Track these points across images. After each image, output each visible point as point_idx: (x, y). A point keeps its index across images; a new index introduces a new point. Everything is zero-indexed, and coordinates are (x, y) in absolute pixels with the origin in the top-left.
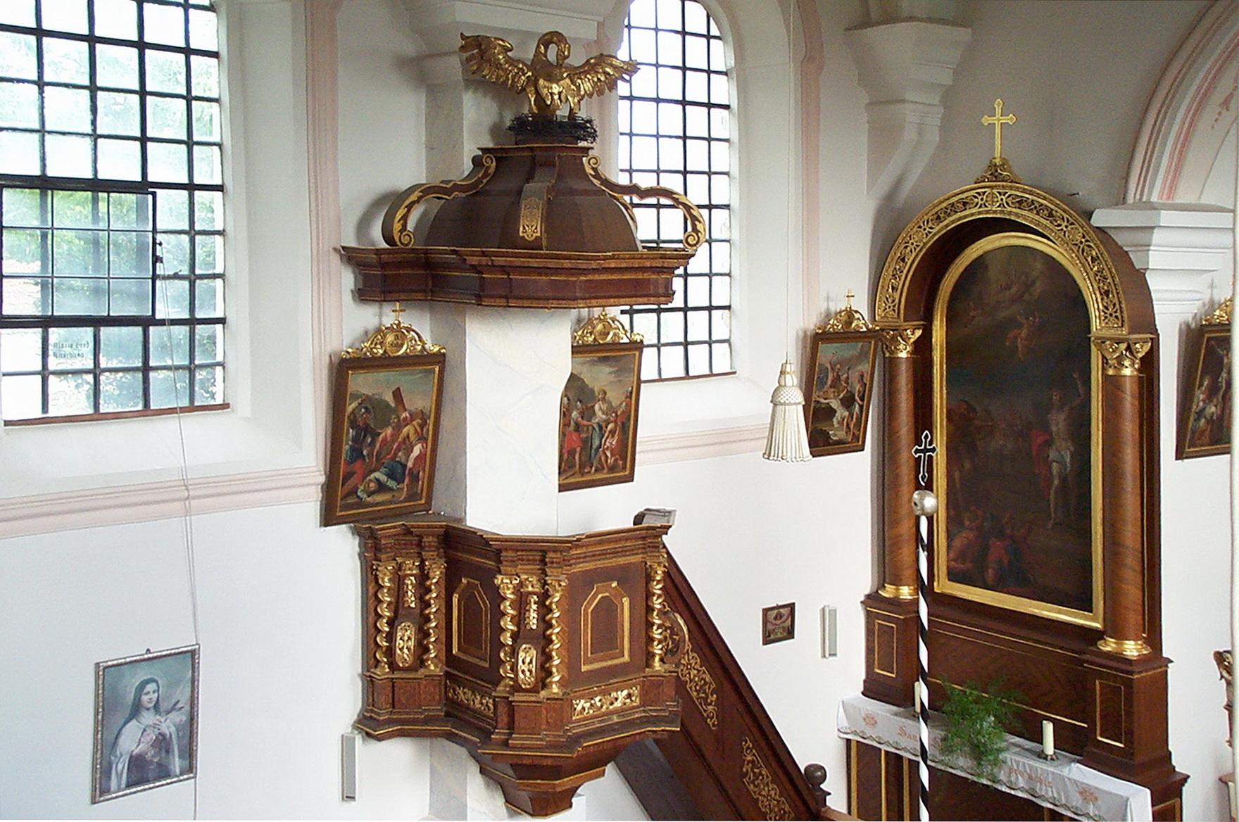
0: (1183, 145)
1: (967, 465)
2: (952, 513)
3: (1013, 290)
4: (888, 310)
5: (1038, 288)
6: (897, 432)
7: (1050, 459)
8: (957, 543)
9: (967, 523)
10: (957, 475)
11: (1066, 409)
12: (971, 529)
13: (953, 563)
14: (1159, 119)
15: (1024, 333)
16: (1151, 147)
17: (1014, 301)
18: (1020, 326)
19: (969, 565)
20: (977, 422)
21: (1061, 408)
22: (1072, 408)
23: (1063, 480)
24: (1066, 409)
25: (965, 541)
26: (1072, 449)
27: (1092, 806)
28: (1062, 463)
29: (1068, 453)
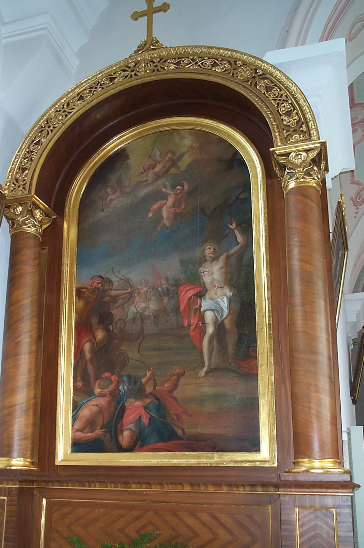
0: (338, 18)
1: (100, 335)
2: (80, 384)
3: (158, 168)
4: (61, 113)
5: (186, 161)
6: (19, 301)
7: (202, 309)
8: (85, 412)
9: (97, 391)
10: (87, 347)
11: (222, 258)
12: (103, 396)
13: (79, 433)
14: (304, 29)
15: (170, 201)
16: (307, 22)
17: (158, 177)
18: (165, 197)
19: (98, 432)
20: (113, 293)
21: (215, 259)
22: (228, 258)
23: (220, 326)
24: (222, 258)
25: (96, 409)
26: (230, 294)
27: (313, 510)
28: (217, 310)
29: (225, 299)
